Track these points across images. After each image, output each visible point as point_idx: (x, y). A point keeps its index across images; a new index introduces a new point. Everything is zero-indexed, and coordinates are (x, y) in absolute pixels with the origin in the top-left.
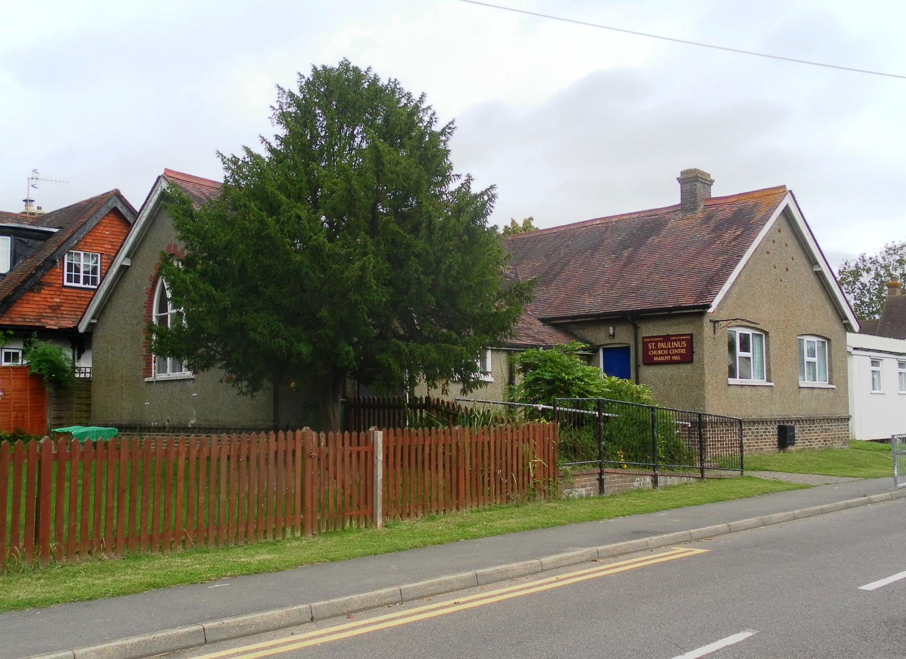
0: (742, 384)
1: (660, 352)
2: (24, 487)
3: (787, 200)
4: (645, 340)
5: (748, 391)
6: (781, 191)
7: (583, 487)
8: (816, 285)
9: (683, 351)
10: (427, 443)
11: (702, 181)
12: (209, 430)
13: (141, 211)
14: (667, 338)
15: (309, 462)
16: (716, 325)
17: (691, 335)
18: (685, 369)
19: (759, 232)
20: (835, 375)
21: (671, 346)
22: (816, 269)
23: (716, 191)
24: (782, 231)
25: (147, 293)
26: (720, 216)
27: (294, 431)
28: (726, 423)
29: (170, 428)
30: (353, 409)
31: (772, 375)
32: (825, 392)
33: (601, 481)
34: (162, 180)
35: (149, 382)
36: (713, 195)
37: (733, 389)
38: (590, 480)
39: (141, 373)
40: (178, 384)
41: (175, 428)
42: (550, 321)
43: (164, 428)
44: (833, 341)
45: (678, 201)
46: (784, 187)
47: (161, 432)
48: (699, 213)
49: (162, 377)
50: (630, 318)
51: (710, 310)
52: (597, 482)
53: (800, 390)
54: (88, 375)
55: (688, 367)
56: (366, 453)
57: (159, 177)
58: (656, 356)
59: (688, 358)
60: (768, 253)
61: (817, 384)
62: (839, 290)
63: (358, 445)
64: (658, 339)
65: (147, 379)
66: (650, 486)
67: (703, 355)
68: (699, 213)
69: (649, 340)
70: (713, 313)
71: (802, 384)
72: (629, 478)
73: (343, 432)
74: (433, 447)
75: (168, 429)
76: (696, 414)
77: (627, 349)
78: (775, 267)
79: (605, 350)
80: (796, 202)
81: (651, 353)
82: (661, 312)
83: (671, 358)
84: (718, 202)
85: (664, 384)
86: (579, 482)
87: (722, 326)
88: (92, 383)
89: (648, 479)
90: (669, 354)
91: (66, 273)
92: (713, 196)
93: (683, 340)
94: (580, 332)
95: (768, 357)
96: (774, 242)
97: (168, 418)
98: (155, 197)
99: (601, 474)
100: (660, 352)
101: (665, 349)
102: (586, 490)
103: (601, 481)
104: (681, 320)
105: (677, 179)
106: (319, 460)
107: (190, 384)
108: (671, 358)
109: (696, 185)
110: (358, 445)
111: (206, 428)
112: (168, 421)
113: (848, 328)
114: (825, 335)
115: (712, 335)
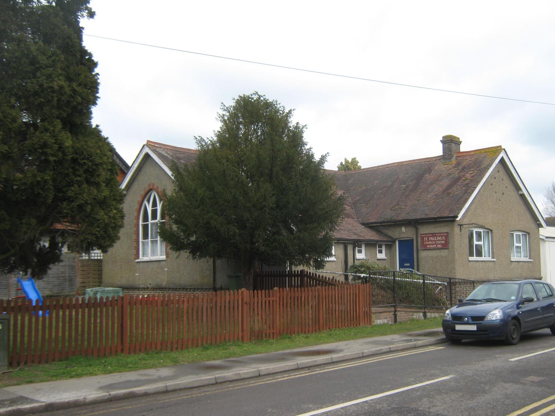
0: (477, 260)
1: (430, 243)
2: (12, 328)
3: (502, 154)
4: (422, 236)
5: (481, 264)
6: (497, 150)
7: (385, 318)
8: (521, 202)
9: (443, 242)
10: (303, 295)
11: (455, 142)
12: (175, 289)
13: (132, 166)
14: (434, 235)
15: (245, 306)
16: (462, 227)
17: (447, 233)
18: (444, 253)
19: (487, 171)
20: (533, 254)
21: (437, 239)
22: (520, 193)
23: (463, 148)
24: (500, 171)
25: (136, 211)
26: (465, 164)
27: (238, 290)
28: (465, 282)
29: (151, 288)
30: (259, 278)
31: (495, 255)
32: (527, 264)
33: (395, 316)
34: (146, 147)
35: (138, 262)
36: (462, 150)
37: (472, 263)
38: (390, 315)
39: (133, 257)
40: (156, 263)
41: (154, 288)
42: (368, 225)
43: (148, 288)
44: (531, 234)
45: (441, 153)
46: (501, 146)
47: (145, 291)
48: (454, 161)
49: (146, 259)
50: (413, 223)
51: (458, 219)
52: (393, 316)
53: (512, 263)
54: (102, 258)
55: (447, 251)
56: (273, 301)
57: (144, 145)
58: (428, 245)
59: (445, 246)
60: (492, 185)
61: (523, 259)
62: (430, 251)
63: (269, 297)
64: (429, 235)
65: (137, 260)
66: (423, 318)
67: (454, 244)
68: (454, 161)
69: (424, 235)
70: (460, 220)
71: (513, 259)
72: (411, 314)
73: (254, 291)
74: (306, 297)
75: (150, 289)
76: (448, 278)
77: (412, 240)
78: (496, 193)
79: (400, 241)
80: (507, 155)
81: (426, 243)
82: (428, 220)
83: (437, 246)
84: (464, 154)
85: (433, 261)
86: (383, 316)
87: (465, 227)
88: (103, 262)
89: (421, 314)
90: (435, 244)
91: (141, 222)
92: (461, 151)
93: (443, 236)
94: (385, 231)
95: (492, 244)
96: (495, 178)
97: (150, 282)
98: (141, 157)
99: (395, 311)
100: (430, 243)
101: (433, 241)
102: (387, 320)
103: (395, 316)
104: (442, 224)
105: (441, 141)
106: (250, 305)
107: (164, 263)
108: (437, 246)
109: (451, 145)
110: (269, 297)
111: (173, 289)
112: (150, 284)
113: (540, 226)
114: (526, 231)
115: (459, 233)
